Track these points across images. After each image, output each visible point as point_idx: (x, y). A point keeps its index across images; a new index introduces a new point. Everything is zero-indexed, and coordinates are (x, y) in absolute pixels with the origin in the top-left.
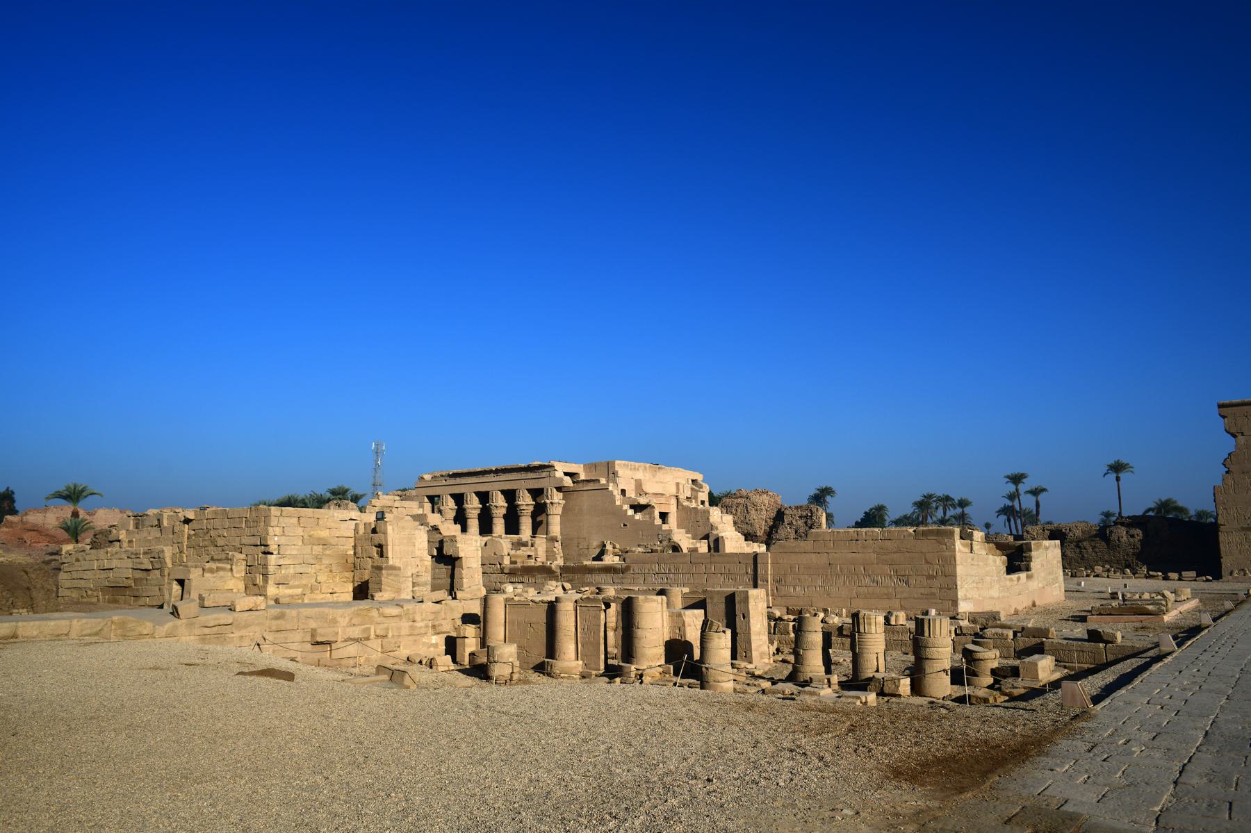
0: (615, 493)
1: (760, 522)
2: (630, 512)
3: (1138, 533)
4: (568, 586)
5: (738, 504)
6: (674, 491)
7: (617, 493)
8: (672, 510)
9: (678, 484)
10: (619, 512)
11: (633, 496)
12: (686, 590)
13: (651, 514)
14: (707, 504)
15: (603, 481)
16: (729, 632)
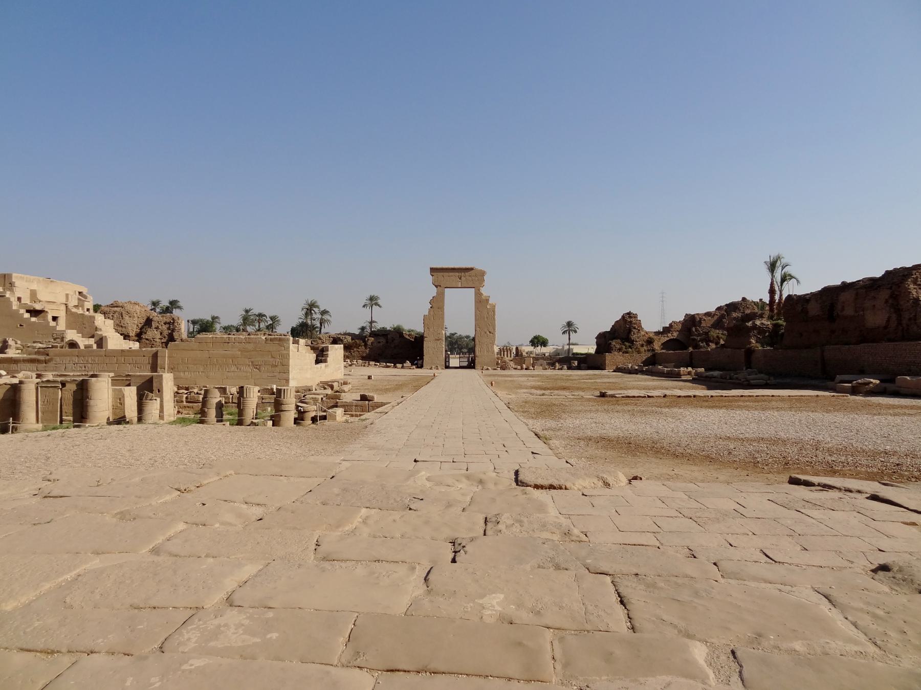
0: (12, 299)
2: (27, 315)
3: (383, 340)
5: (115, 312)
7: (14, 300)
8: (62, 314)
9: (67, 295)
10: (15, 315)
11: (28, 302)
12: (112, 374)
13: (45, 319)
14: (92, 311)
16: (158, 399)
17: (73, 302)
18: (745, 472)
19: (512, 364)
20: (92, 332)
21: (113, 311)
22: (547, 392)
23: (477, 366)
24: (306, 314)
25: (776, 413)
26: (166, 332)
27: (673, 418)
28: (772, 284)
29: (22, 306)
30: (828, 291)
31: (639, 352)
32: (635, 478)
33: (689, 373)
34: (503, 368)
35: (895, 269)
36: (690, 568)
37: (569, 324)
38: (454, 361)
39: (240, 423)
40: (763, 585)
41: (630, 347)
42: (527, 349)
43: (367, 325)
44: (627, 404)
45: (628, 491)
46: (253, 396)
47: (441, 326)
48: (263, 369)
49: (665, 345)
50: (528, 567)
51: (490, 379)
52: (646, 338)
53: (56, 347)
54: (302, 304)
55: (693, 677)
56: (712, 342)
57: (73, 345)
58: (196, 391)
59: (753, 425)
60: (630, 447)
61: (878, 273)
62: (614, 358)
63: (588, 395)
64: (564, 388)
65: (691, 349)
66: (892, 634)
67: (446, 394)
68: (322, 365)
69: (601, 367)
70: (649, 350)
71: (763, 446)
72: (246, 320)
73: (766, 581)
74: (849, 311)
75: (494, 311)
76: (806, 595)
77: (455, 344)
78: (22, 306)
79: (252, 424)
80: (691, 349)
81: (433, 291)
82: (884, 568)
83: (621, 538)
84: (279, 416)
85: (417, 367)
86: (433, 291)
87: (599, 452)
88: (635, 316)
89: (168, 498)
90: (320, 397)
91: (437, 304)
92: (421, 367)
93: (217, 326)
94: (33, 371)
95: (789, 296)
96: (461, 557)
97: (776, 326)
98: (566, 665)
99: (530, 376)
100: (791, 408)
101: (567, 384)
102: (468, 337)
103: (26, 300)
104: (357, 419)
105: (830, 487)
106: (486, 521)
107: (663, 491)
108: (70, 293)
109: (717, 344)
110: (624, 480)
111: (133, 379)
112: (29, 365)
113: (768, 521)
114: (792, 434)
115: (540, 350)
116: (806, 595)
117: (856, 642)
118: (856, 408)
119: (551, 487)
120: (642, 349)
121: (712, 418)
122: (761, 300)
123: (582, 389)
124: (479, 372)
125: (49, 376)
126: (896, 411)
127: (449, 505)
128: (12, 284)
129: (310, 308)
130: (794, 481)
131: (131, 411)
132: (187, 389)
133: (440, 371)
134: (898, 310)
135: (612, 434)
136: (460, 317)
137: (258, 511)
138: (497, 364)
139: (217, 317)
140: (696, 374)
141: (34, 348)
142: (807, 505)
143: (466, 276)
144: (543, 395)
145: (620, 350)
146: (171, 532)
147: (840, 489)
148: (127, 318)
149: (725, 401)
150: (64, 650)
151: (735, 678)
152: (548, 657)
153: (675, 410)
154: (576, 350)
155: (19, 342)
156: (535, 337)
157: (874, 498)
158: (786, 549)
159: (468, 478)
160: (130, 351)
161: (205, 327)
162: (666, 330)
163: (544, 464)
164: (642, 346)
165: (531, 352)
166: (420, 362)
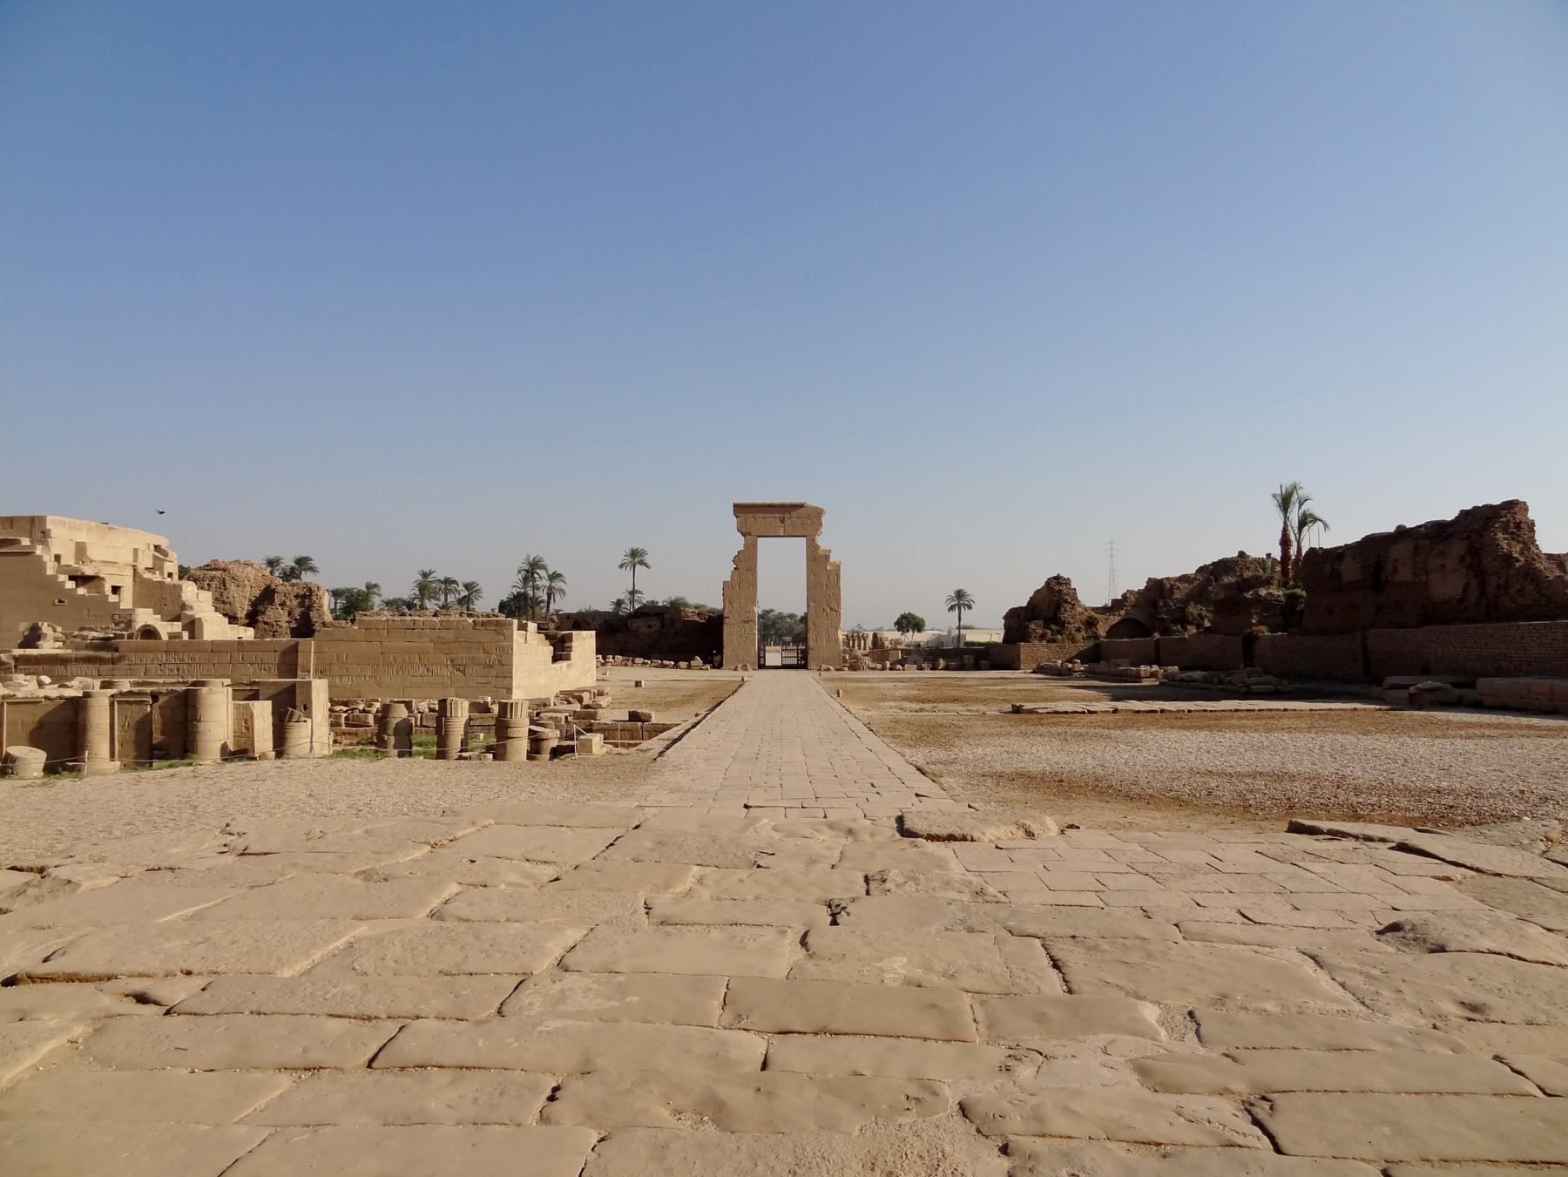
0: (46, 558)
1: (242, 603)
2: (70, 585)
3: (656, 623)
4: (46, 679)
5: (212, 578)
6: (130, 559)
9: (136, 551)
11: (72, 562)
13: (100, 589)
14: (176, 577)
15: (25, 542)
17: (146, 561)
18: (1230, 819)
19: (867, 660)
20: (178, 612)
21: (213, 577)
22: (928, 706)
23: (812, 664)
24: (525, 580)
25: (1286, 736)
26: (297, 612)
27: (1128, 744)
28: (1285, 531)
29: (62, 569)
30: (1374, 545)
31: (1073, 640)
32: (1071, 827)
33: (1153, 675)
34: (854, 668)
35: (1475, 508)
36: (1143, 929)
37: (960, 595)
38: (774, 656)
39: (442, 755)
40: (1236, 947)
41: (1059, 632)
42: (891, 635)
43: (624, 596)
44: (1055, 724)
45: (1061, 843)
46: (461, 712)
47: (753, 600)
48: (469, 671)
49: (1112, 632)
50: (933, 930)
51: (837, 685)
52: (1083, 618)
53: (122, 637)
54: (520, 562)
55: (1142, 1035)
56: (1191, 623)
57: (149, 633)
58: (361, 707)
59: (1250, 755)
60: (1060, 787)
61: (1450, 515)
62: (1034, 650)
63: (992, 710)
64: (955, 700)
65: (1157, 635)
66: (1386, 993)
67: (768, 715)
68: (563, 664)
69: (1012, 665)
70: (1089, 638)
71: (1260, 783)
72: (424, 589)
73: (1239, 943)
74: (1405, 575)
75: (838, 575)
76: (1288, 956)
77: (772, 629)
78: (62, 569)
79: (460, 758)
80: (1157, 635)
81: (739, 542)
82: (1395, 927)
83: (1051, 898)
84: (504, 746)
85: (713, 667)
86: (739, 542)
87: (1016, 794)
88: (1067, 582)
89: (417, 854)
90: (563, 716)
91: (745, 563)
92: (720, 666)
93: (377, 601)
94: (93, 677)
95: (1312, 550)
96: (842, 918)
97: (1292, 598)
98: (990, 1027)
99: (898, 680)
100: (1309, 729)
101: (955, 693)
102: (792, 616)
103: (69, 560)
104: (633, 750)
105: (1344, 835)
106: (867, 879)
107: (1109, 842)
108: (141, 547)
109: (1198, 627)
110: (1054, 829)
111: (263, 691)
112: (92, 668)
113: (1248, 876)
114: (1306, 767)
115: (912, 637)
116: (1288, 956)
117: (1338, 1001)
118: (1409, 729)
119: (951, 838)
120: (1079, 636)
121: (1188, 743)
122: (1269, 555)
123: (984, 701)
124: (815, 674)
125: (125, 685)
126: (1471, 731)
127: (812, 862)
128: (45, 534)
129: (532, 568)
130: (1296, 828)
131: (263, 738)
132: (345, 704)
133: (751, 672)
134: (1480, 574)
135: (1034, 768)
136: (782, 584)
137: (551, 872)
138: (845, 661)
139: (375, 586)
140: (1166, 676)
141: (84, 638)
142: (1307, 857)
143: (792, 518)
144: (921, 710)
145: (1042, 637)
146: (445, 895)
147: (1356, 838)
148: (232, 587)
149: (1209, 719)
150: (383, 1015)
151: (1191, 1035)
152: (970, 1018)
153: (1131, 732)
154: (971, 637)
155: (59, 629)
156: (904, 617)
157: (1403, 847)
158: (1274, 909)
159: (831, 826)
160: (240, 643)
161: (353, 604)
162: (1117, 605)
163: (936, 808)
164: (1079, 630)
165: (897, 642)
166: (717, 659)
